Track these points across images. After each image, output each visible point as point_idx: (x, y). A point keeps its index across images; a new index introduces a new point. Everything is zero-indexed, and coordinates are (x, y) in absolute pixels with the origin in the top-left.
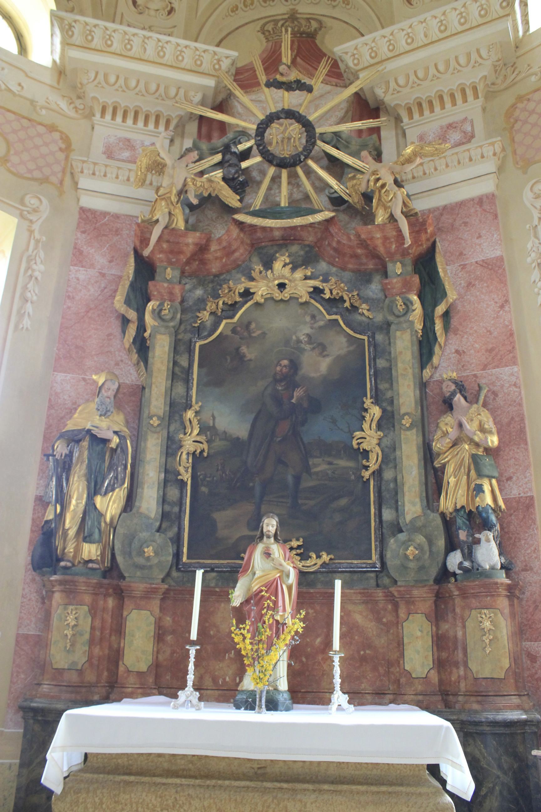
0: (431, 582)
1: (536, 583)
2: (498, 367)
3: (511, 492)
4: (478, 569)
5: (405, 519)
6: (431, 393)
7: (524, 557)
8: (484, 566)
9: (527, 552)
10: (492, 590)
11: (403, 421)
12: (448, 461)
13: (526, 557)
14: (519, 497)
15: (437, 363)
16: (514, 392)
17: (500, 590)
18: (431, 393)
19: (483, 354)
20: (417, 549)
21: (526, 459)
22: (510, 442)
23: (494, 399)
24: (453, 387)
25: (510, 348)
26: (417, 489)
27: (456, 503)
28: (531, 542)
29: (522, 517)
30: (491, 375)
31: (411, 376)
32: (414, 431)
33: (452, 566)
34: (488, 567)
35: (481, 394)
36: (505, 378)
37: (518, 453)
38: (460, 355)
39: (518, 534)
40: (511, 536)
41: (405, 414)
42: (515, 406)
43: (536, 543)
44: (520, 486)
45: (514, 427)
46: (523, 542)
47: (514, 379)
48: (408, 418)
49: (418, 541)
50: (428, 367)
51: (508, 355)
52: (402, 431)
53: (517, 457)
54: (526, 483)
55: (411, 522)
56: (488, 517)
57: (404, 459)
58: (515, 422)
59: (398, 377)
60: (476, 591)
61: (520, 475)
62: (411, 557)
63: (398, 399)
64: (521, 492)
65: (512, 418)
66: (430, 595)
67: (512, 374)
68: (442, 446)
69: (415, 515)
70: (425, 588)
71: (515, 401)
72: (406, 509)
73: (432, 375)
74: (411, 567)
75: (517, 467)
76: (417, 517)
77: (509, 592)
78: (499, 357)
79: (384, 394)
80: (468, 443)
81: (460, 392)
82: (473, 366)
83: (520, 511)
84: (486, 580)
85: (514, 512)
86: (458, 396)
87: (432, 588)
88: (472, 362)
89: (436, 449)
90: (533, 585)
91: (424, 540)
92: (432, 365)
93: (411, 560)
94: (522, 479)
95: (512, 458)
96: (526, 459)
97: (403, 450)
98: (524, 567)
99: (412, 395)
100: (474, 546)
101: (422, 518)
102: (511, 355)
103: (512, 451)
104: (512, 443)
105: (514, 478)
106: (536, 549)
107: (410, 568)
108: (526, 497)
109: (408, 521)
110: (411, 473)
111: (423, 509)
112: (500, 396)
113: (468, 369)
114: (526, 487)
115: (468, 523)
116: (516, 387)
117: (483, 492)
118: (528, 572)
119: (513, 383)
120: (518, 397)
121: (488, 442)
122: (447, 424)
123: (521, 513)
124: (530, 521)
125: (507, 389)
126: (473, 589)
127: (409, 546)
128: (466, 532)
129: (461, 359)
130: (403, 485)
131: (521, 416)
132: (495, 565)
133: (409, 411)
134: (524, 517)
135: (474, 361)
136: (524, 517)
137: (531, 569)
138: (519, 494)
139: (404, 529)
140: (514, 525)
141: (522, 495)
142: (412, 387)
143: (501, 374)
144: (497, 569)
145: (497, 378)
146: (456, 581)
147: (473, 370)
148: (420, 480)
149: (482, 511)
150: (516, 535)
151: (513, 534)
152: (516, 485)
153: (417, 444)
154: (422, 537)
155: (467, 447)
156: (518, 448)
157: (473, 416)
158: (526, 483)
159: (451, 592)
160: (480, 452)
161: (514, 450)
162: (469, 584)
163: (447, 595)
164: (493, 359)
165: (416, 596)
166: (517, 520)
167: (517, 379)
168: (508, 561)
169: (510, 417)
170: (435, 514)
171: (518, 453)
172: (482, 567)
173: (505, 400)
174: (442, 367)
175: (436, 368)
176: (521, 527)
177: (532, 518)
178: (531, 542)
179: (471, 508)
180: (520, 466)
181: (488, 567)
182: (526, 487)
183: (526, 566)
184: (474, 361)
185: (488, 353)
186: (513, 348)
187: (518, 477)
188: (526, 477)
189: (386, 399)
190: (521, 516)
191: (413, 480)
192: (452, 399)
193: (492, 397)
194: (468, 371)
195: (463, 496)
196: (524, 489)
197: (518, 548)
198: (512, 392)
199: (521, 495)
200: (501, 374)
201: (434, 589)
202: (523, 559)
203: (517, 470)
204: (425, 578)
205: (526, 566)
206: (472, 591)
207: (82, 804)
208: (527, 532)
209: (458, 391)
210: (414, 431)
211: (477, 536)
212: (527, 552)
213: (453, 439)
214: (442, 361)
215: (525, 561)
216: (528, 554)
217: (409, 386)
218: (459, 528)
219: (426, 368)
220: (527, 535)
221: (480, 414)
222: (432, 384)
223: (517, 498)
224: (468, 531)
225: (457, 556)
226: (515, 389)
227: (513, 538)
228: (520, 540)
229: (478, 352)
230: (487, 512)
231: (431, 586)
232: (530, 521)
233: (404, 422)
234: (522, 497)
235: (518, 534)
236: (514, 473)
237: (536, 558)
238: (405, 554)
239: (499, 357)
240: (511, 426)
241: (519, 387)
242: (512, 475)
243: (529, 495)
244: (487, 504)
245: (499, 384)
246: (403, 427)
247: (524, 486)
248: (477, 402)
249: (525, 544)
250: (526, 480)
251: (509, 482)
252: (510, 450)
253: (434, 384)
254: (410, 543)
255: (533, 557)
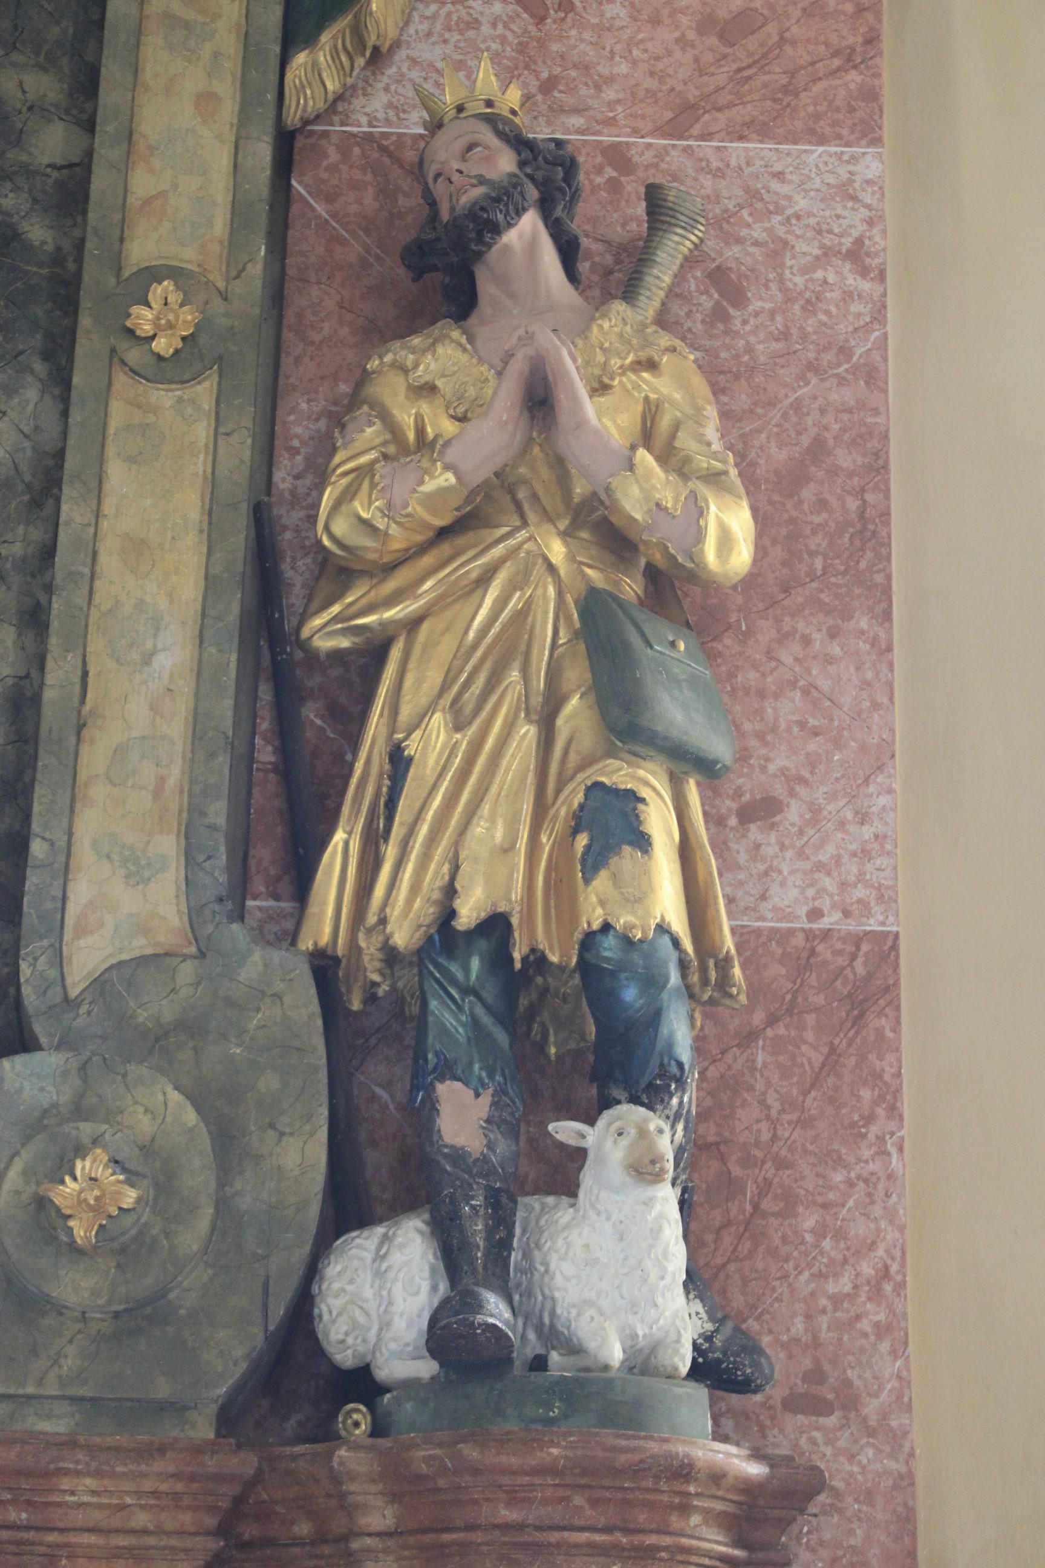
0: (203, 1429)
1: (868, 1497)
2: (764, 133)
3: (763, 897)
4: (539, 1364)
5: (59, 960)
6: (320, 209)
7: (808, 1317)
8: (592, 1345)
9: (832, 1288)
10: (642, 1517)
11: (137, 310)
12: (414, 623)
13: (824, 1321)
14: (809, 935)
15: (392, 33)
16: (849, 296)
17: (695, 1519)
18: (320, 209)
19: (682, 42)
20: (132, 1177)
21: (876, 706)
22: (786, 590)
23: (719, 315)
24: (506, 163)
25: (855, 39)
26: (175, 774)
27: (450, 891)
28: (860, 1229)
29: (817, 1059)
30: (718, 174)
31: (229, 43)
32: (204, 391)
33: (355, 1325)
34: (615, 1354)
35: (661, 256)
36: (802, 203)
37: (829, 660)
38: (541, 20)
39: (782, 1164)
40: (736, 1171)
41: (153, 274)
42: (842, 381)
43: (892, 1235)
44: (819, 867)
45: (822, 504)
46: (809, 1220)
47: (854, 220)
48: (174, 298)
49: (145, 1126)
50: (325, 38)
51: (834, 73)
52: (121, 379)
53: (825, 684)
54: (864, 854)
55: (100, 984)
56: (655, 1017)
57: (109, 561)
58: (834, 472)
59: (139, 33)
60: (532, 1515)
61: (832, 797)
62: (81, 1231)
63: (125, 167)
64: (825, 904)
65: (818, 450)
66: (186, 1519)
67: (846, 192)
68: (389, 511)
69: (140, 946)
70: (159, 1465)
71: (845, 352)
72: (80, 892)
73: (340, 98)
74: (72, 1299)
75: (812, 746)
76: (143, 961)
77: (739, 1542)
78: (776, 75)
79: (19, 140)
80: (563, 524)
81: (545, 206)
82: (610, 94)
83: (810, 1019)
84: (609, 1437)
85: (772, 1020)
86: (530, 222)
87: (212, 1463)
88: (604, 69)
89: (340, 527)
90: (852, 1505)
91: (191, 1117)
92: (357, 31)
93: (76, 1250)
94: (842, 824)
95: (793, 684)
96: (876, 706)
97: (107, 508)
98: (801, 1388)
99: (222, 160)
100: (529, 1206)
101: (187, 971)
102: (854, 78)
103: (796, 648)
104: (798, 597)
105: (794, 813)
106: (885, 1274)
107: (60, 1310)
108: (858, 940)
109: (79, 972)
110: (148, 659)
111: (195, 914)
112: (757, 304)
113: (577, 111)
114: (861, 877)
115: (502, 1037)
116: (864, 272)
117: (643, 842)
118: (831, 1421)
119: (847, 242)
120: (867, 328)
121: (700, 537)
122: (428, 390)
123: (809, 1036)
124: (866, 1094)
125: (803, 271)
126: (514, 1499)
127: (80, 1151)
128: (486, 1098)
129: (542, 43)
130: (81, 727)
131: (873, 444)
132: (655, 1346)
133: (187, 256)
134: (832, 1060)
135: (624, 68)
136: (832, 1060)
137: (849, 1401)
138: (815, 914)
139: (40, 1028)
140: (763, 1103)
141: (831, 920)
142: (229, 110)
143: (779, 176)
144: (671, 1376)
145: (754, 195)
146: (378, 1430)
147: (610, 122)
148: (199, 719)
149: (622, 967)
150: (769, 1170)
151: (747, 1161)
152: (801, 855)
153: (213, 481)
154: (175, 1096)
155: (557, 550)
156: (833, 634)
157: (615, 363)
158: (864, 854)
159: (345, 1505)
160: (631, 587)
161: (806, 641)
162: (492, 1458)
163: (303, 1529)
164: (740, 78)
165: (79, 1518)
166: (785, 1073)
167: (870, 223)
168: (728, 1329)
169: (806, 441)
170: (277, 956)
171: (829, 660)
172: (574, 1349)
173: (785, 335)
174: (414, 61)
175: (377, 58)
176: (805, 1123)
177: (878, 1076)
178: (860, 1229)
179: (543, 945)
180: (838, 743)
181: (615, 1354)
182: (861, 877)
183: (816, 1375)
184: (624, 68)
185: (713, 41)
186: (872, 39)
187: (816, 810)
188: (863, 818)
189: (29, 171)
190: (812, 1056)
191: (155, 708)
192: (496, 230)
193: (707, 303)
194: (577, 121)
195: (508, 849)
196: (843, 886)
197: (773, 1252)
198: (835, 295)
199: (825, 923)
200: (779, 176)
201: (219, 1478)
202: (799, 1327)
203: (813, 760)
204: (162, 1389)
205: (816, 1375)
206: (508, 1514)
207: (769, 442)
208: (839, 1162)
209: (533, 193)
210: (204, 391)
211: (565, 1130)
212: (832, 1288)
213: (477, 478)
214: (418, 26)
215: (816, 1343)
216: (837, 1301)
217: (206, 101)
218: (447, 1070)
219: (310, 41)
220: (838, 1177)
221: (651, 365)
222: (333, 156)
223: (799, 941)
224: (500, 1092)
225: (396, 1258)
226: (852, 281)
227: (750, 1190)
228: (790, 1203)
229: (655, 21)
230: (653, 982)
231: (197, 1450)
232: (866, 1094)
233: (143, 319)
234: (826, 934)
235: (782, 1164)
236: (794, 780)
237: (881, 1330)
238: (42, 1203)
239: (776, 75)
240: (808, 493)
241: (882, 277)
242: (779, 790)
243: (872, 925)
244: (662, 928)
245: (758, 233)
246: (133, 355)
247: (851, 868)
248: (629, 291)
249: (820, 1232)
250: (867, 832)
251: (754, 832)
252: (784, 638)
253: (345, 152)
254: (87, 1129)
255: (865, 1325)
